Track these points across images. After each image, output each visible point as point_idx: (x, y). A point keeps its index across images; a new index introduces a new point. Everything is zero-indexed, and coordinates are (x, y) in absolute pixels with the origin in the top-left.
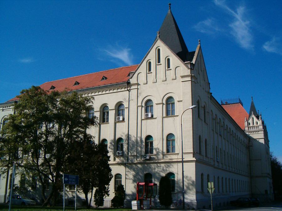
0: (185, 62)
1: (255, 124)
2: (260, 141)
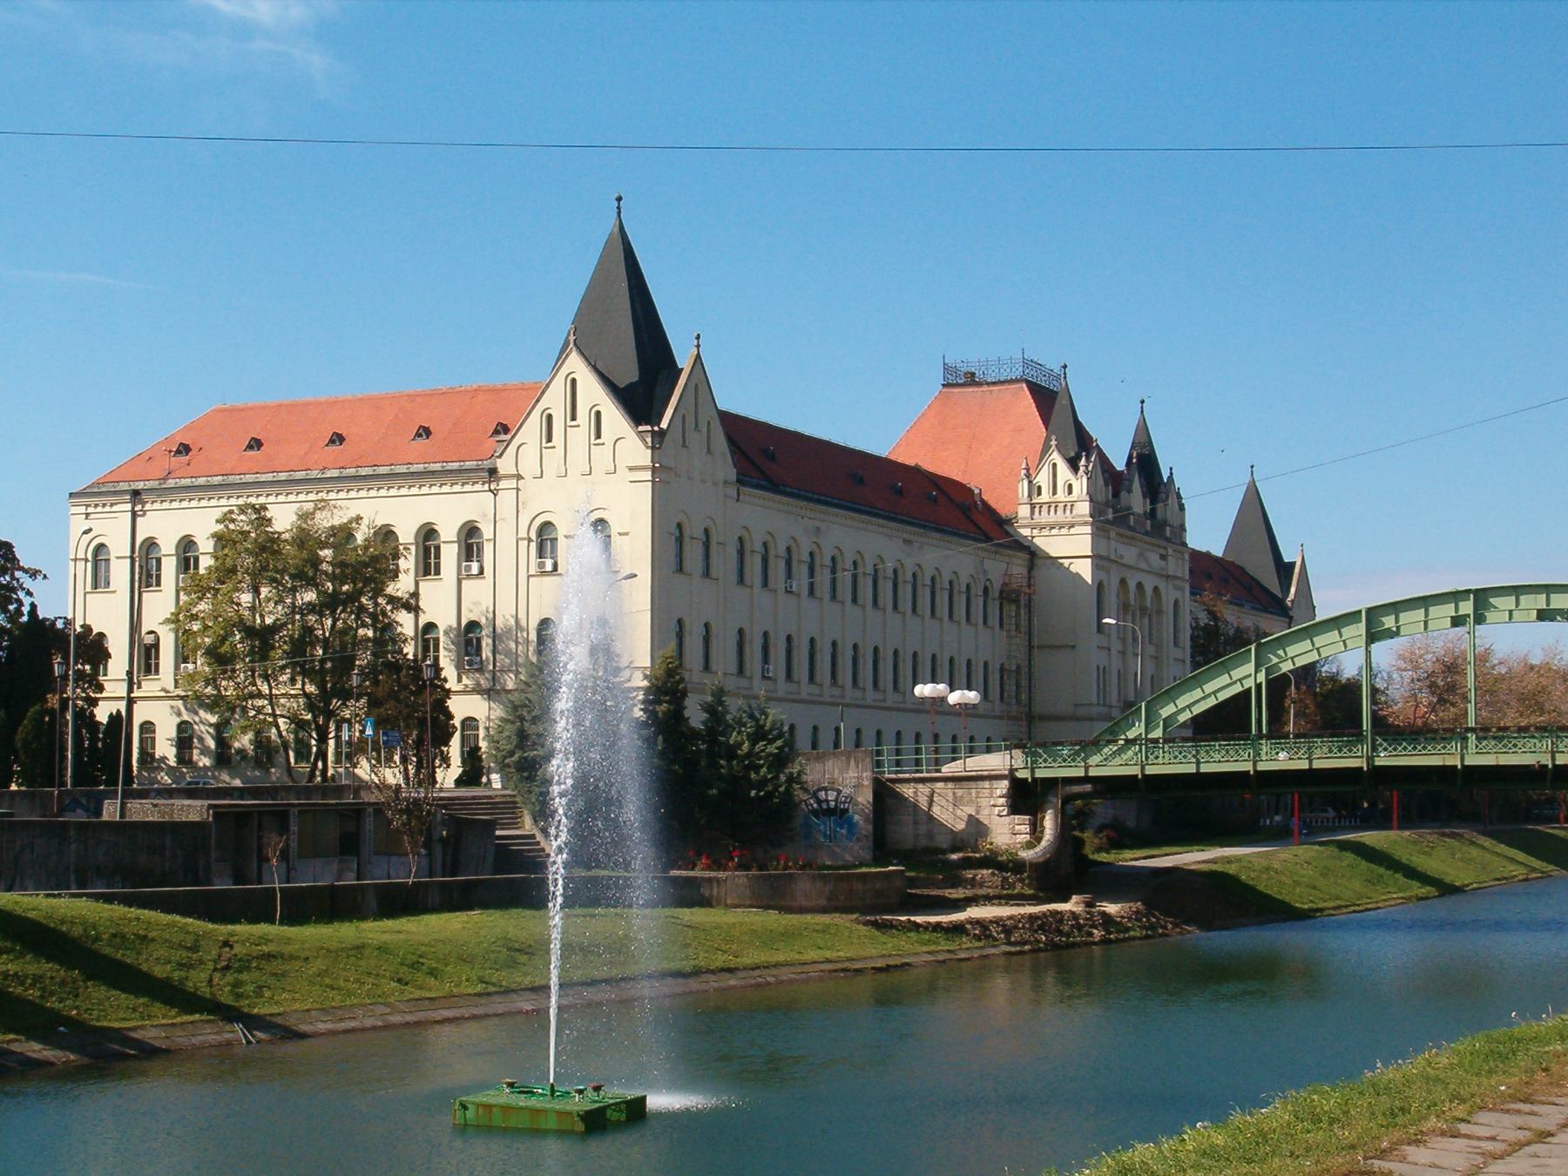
0: (641, 428)
1: (1061, 495)
2: (1073, 569)
